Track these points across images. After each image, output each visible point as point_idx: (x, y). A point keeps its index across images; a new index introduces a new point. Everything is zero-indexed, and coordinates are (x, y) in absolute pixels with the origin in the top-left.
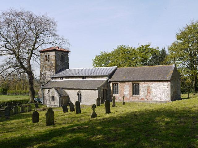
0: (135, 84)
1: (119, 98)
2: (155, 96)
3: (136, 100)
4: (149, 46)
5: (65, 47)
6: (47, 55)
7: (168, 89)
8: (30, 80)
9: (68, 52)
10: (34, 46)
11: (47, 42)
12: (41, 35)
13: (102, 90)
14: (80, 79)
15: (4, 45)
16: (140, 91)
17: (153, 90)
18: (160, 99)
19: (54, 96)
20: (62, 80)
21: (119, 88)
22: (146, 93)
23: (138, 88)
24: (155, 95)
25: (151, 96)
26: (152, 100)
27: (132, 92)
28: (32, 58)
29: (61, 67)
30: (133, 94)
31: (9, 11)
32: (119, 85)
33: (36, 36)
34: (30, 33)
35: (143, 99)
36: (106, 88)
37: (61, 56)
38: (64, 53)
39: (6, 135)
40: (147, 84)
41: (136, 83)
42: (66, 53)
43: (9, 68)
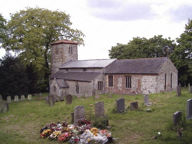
1: (114, 91)
4: (162, 36)
7: (156, 82)
13: (96, 83)
14: (81, 71)
16: (132, 84)
17: (143, 83)
18: (149, 92)
21: (113, 84)
22: (137, 86)
24: (144, 88)
25: (141, 90)
27: (125, 85)
29: (69, 60)
31: (26, 10)
36: (101, 80)
37: (69, 48)
38: (72, 45)
40: (138, 77)
42: (75, 45)
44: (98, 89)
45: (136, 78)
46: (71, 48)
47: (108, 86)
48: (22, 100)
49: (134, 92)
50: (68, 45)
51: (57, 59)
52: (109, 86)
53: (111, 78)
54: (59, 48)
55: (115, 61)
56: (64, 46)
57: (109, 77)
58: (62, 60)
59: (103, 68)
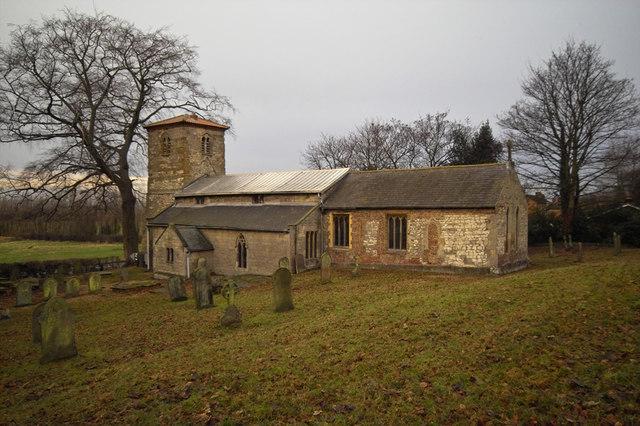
0: (394, 219)
2: (451, 253)
3: (397, 262)
5: (219, 115)
6: (166, 136)
8: (124, 203)
9: (223, 129)
10: (137, 113)
11: (171, 102)
12: (158, 84)
13: (302, 235)
14: (249, 203)
15: (46, 106)
16: (409, 238)
17: (445, 235)
18: (466, 260)
20: (200, 206)
21: (351, 229)
23: (405, 229)
25: (440, 253)
26: (444, 264)
27: (386, 242)
28: (133, 146)
29: (204, 171)
30: (391, 246)
33: (143, 87)
34: (123, 76)
35: (415, 261)
36: (313, 228)
37: (203, 139)
38: (210, 132)
39: (161, 250)
41: (398, 216)
42: (219, 133)
43: (67, 171)
45: (423, 220)
47: (331, 245)
50: (200, 132)
51: (165, 170)
52: (336, 243)
55: (347, 176)
59: (316, 194)
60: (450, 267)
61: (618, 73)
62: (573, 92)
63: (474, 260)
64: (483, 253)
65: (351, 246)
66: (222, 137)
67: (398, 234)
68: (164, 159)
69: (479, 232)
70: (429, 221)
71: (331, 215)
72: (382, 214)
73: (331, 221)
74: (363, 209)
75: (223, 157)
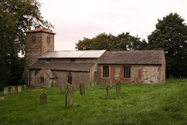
7: (159, 72)
9: (54, 34)
16: (131, 74)
17: (144, 73)
18: (151, 82)
19: (43, 78)
21: (110, 71)
22: (137, 76)
25: (142, 79)
27: (123, 76)
30: (124, 77)
32: (110, 68)
37: (48, 37)
38: (50, 35)
42: (52, 36)
44: (41, 81)
46: (49, 38)
47: (102, 77)
48: (12, 92)
49: (134, 82)
50: (46, 35)
52: (104, 76)
53: (106, 68)
54: (36, 36)
55: (105, 52)
56: (43, 35)
57: (104, 68)
58: (40, 49)
60: (146, 84)
61: (183, 18)
62: (171, 23)
63: (154, 82)
64: (157, 79)
65: (109, 77)
66: (53, 37)
67: (127, 73)
68: (33, 44)
69: (156, 72)
70: (138, 69)
71: (102, 66)
72: (121, 66)
73: (102, 68)
74: (114, 64)
75: (54, 45)
